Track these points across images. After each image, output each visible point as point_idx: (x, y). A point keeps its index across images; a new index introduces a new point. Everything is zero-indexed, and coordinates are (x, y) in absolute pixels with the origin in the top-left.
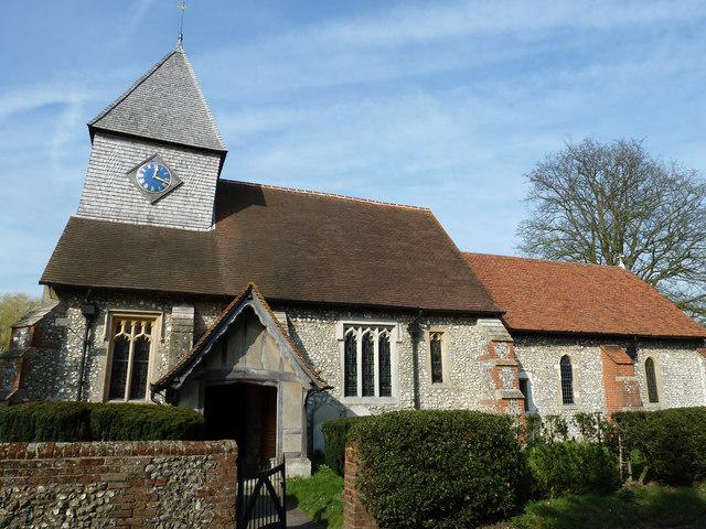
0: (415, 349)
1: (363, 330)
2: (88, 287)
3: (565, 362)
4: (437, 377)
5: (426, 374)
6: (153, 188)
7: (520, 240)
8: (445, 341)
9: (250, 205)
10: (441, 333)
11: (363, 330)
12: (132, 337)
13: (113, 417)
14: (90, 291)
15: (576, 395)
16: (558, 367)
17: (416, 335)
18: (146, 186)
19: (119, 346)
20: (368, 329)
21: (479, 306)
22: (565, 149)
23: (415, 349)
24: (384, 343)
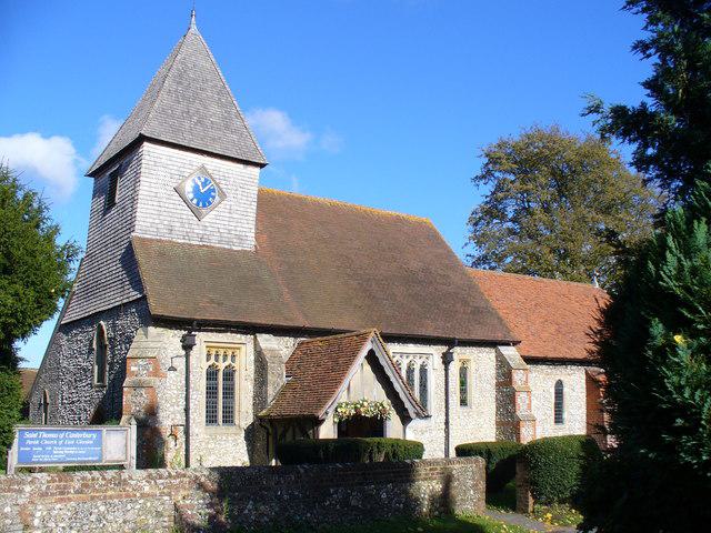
0: (446, 370)
2: (194, 320)
3: (559, 385)
4: (463, 402)
5: (455, 398)
6: (201, 205)
7: (647, 68)
8: (472, 367)
9: (23, 132)
10: (468, 360)
12: (222, 366)
13: (647, 248)
14: (195, 323)
15: (565, 415)
16: (553, 391)
17: (447, 359)
18: (195, 201)
19: (212, 374)
20: (411, 358)
21: (499, 336)
22: (637, 105)
23: (446, 370)
24: (423, 371)
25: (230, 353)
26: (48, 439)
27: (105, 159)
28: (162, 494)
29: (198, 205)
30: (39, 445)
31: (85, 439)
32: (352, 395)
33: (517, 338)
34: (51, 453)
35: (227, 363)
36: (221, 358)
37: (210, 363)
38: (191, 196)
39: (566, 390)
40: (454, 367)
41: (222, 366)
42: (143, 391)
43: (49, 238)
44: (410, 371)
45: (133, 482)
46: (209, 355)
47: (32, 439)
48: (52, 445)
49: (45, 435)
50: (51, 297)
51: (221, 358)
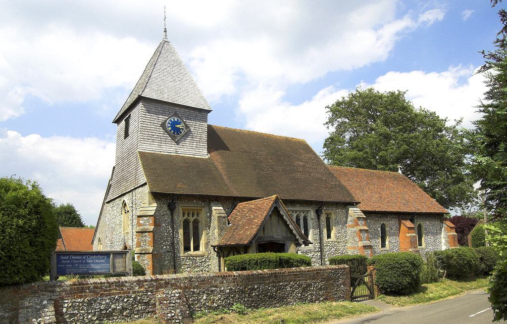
1: (303, 213)
10: (331, 213)
11: (303, 213)
12: (192, 219)
16: (379, 229)
17: (318, 213)
18: (172, 131)
21: (348, 200)
24: (305, 220)
25: (196, 212)
26: (76, 260)
27: (126, 107)
28: (147, 291)
29: (174, 133)
30: (70, 263)
31: (78, 259)
32: (265, 233)
33: (360, 200)
34: (78, 268)
35: (194, 218)
36: (191, 215)
37: (185, 218)
38: (170, 128)
39: (387, 229)
40: (323, 218)
41: (192, 219)
42: (147, 234)
43: (481, 122)
44: (298, 220)
45: (127, 284)
46: (184, 215)
47: (65, 260)
48: (77, 263)
49: (73, 257)
50: (460, 179)
51: (191, 215)
